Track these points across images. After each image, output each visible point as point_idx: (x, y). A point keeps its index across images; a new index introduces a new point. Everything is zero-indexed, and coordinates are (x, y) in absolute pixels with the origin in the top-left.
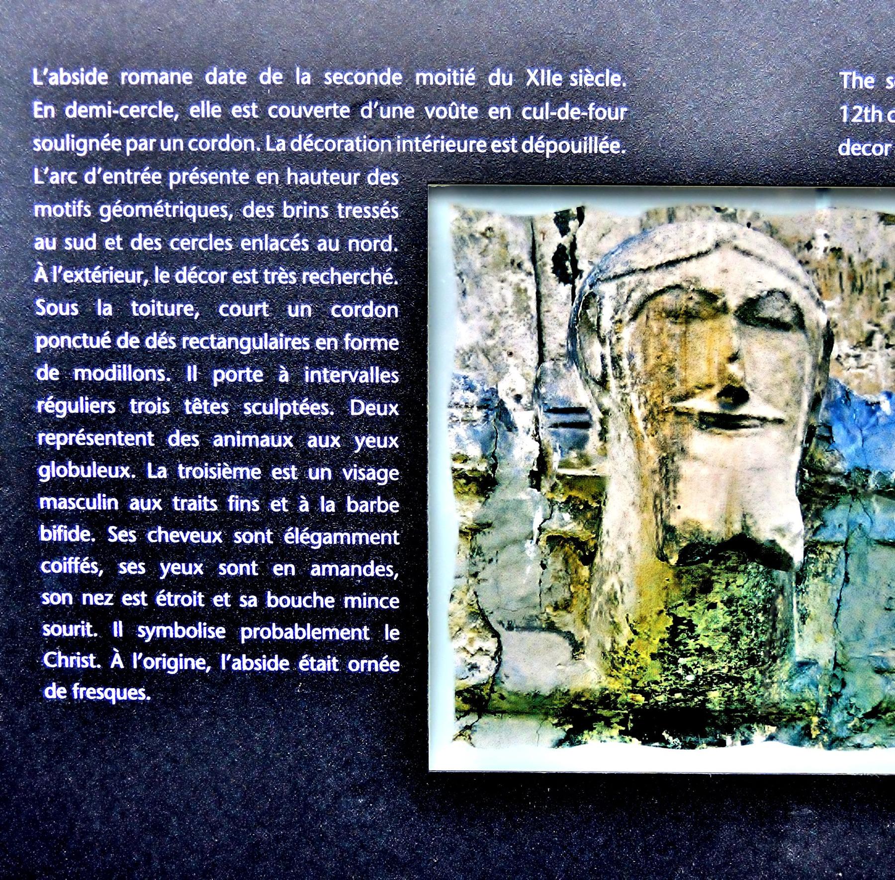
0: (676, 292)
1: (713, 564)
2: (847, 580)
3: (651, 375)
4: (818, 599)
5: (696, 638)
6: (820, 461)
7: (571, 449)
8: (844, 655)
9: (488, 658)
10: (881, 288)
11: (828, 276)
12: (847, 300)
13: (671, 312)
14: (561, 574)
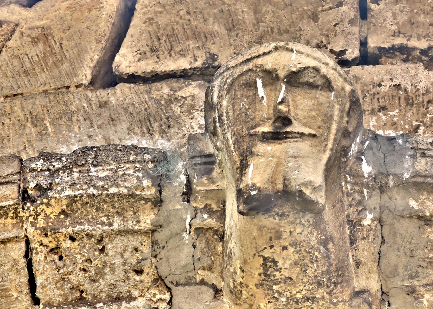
0: (250, 73)
1: (280, 220)
2: (383, 242)
3: (236, 119)
4: (366, 253)
5: (279, 270)
6: (356, 170)
7: (203, 175)
8: (387, 287)
9: (166, 304)
10: (425, 103)
11: (391, 100)
12: (403, 111)
13: (247, 84)
14: (205, 250)
